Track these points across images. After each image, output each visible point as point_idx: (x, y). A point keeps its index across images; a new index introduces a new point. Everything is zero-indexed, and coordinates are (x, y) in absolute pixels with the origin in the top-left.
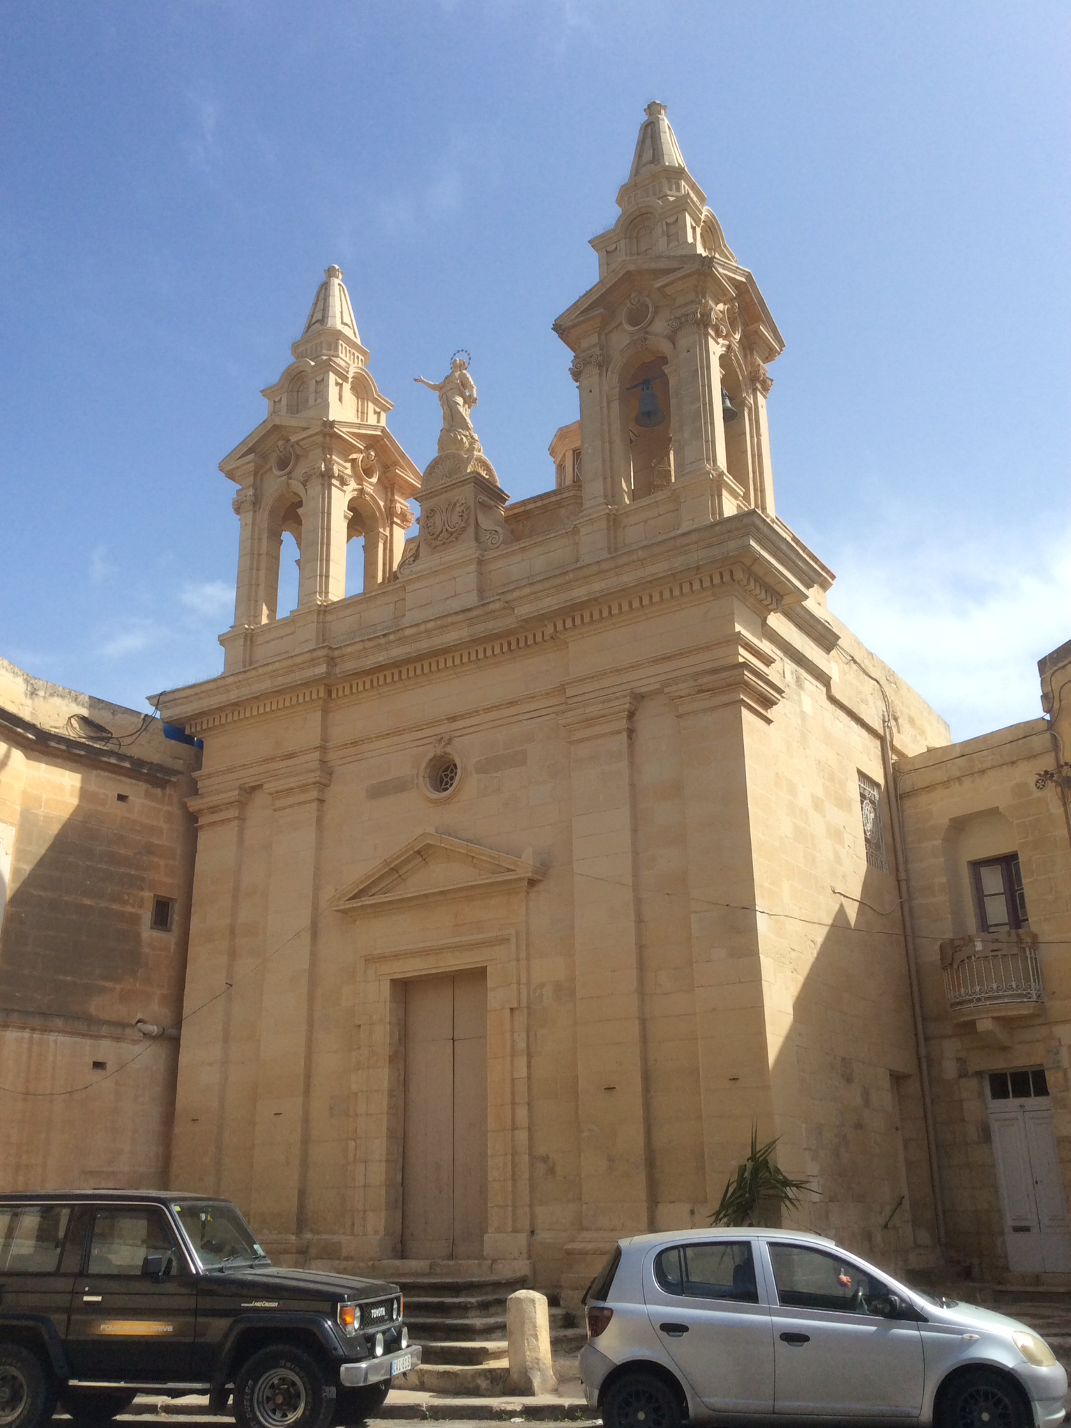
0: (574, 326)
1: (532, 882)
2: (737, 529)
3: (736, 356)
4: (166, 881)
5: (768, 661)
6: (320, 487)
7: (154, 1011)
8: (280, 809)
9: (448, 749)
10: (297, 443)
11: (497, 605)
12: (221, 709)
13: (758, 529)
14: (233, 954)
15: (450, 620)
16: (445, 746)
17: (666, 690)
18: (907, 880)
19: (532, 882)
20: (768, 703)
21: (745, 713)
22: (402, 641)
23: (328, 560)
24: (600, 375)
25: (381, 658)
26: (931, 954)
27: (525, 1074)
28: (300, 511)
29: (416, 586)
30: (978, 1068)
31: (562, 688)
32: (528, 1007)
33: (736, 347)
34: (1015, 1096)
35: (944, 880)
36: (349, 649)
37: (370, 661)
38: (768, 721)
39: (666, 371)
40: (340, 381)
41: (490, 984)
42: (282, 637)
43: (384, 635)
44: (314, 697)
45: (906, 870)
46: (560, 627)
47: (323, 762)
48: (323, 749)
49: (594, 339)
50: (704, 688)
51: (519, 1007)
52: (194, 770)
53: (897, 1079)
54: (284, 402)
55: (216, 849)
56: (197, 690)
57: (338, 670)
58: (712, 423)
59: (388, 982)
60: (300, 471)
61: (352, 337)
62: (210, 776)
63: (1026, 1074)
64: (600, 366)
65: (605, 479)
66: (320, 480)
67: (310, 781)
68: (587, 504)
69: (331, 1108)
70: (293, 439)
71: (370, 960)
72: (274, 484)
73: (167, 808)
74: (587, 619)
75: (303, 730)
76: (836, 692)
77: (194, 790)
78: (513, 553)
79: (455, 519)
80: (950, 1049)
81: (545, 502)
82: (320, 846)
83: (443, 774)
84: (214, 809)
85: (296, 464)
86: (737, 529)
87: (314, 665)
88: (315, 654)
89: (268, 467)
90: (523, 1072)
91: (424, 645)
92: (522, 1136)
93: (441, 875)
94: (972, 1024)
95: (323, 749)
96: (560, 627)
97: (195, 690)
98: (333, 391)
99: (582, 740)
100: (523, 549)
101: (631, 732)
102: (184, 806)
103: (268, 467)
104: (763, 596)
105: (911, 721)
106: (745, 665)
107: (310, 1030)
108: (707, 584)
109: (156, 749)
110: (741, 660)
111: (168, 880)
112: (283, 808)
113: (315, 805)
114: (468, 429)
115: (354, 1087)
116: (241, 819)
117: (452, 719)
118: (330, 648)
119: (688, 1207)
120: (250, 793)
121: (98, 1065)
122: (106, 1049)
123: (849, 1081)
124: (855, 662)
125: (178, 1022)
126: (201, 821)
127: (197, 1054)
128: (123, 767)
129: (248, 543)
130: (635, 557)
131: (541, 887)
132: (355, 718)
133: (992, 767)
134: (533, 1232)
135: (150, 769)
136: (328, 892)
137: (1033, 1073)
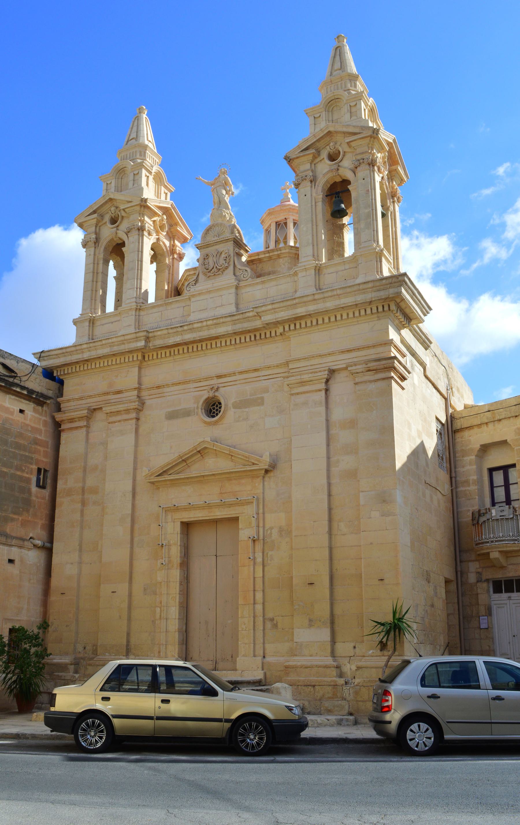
0: (297, 158)
1: (267, 471)
2: (395, 283)
3: (385, 183)
4: (46, 462)
5: (404, 356)
6: (137, 236)
7: (38, 533)
8: (112, 423)
9: (216, 394)
10: (124, 210)
11: (251, 314)
12: (77, 363)
13: (406, 283)
14: (84, 503)
15: (221, 320)
16: (214, 392)
17: (349, 369)
18: (455, 477)
19: (267, 471)
20: (403, 379)
21: (394, 384)
22: (192, 330)
23: (141, 279)
24: (311, 187)
25: (178, 339)
26: (467, 518)
27: (261, 575)
28: (124, 249)
29: (198, 298)
30: (487, 578)
31: (287, 363)
32: (263, 540)
33: (386, 177)
34: (506, 592)
35: (475, 477)
36: (159, 333)
37: (171, 341)
38: (403, 389)
39: (350, 189)
40: (148, 174)
41: (240, 526)
42: (112, 323)
43: (181, 326)
44: (135, 359)
45: (455, 472)
46: (287, 328)
47: (138, 397)
48: (139, 389)
49: (308, 166)
50: (371, 368)
51: (258, 539)
52: (58, 397)
53: (447, 582)
54: (113, 185)
55: (72, 444)
56: (64, 351)
57: (151, 345)
58: (377, 221)
59: (179, 523)
60: (124, 226)
61: (152, 148)
62: (68, 401)
63: (513, 580)
64: (311, 182)
65: (313, 246)
66: (137, 232)
67: (132, 407)
68: (301, 259)
69: (145, 590)
70: (122, 207)
71: (167, 510)
72: (108, 232)
73: (44, 418)
74: (303, 325)
75: (127, 378)
76: (428, 374)
77: (59, 409)
78: (257, 283)
79: (222, 261)
80: (473, 567)
81: (271, 254)
82: (136, 445)
83: (213, 408)
84: (72, 420)
85: (121, 222)
86: (395, 283)
87: (137, 341)
88: (138, 335)
89: (104, 221)
90: (259, 573)
91: (205, 334)
92: (259, 607)
93: (212, 464)
94: (488, 554)
95: (139, 389)
96: (287, 328)
97: (64, 351)
98: (144, 179)
99: (298, 394)
100: (263, 282)
101: (327, 390)
102: (53, 418)
103: (104, 221)
104: (403, 320)
105: (458, 390)
106: (395, 358)
107: (132, 547)
108: (374, 310)
109: (38, 384)
110: (393, 355)
111: (45, 460)
112: (115, 422)
113: (134, 421)
114: (228, 209)
115: (159, 579)
116: (88, 427)
117: (219, 377)
118: (147, 332)
119: (352, 645)
120: (93, 412)
121: (11, 561)
122: (15, 552)
123: (429, 582)
124: (436, 356)
125: (51, 539)
126: (63, 427)
127: (63, 557)
128: (23, 394)
129: (91, 266)
130: (335, 293)
131: (271, 474)
132: (161, 372)
133: (505, 418)
134: (264, 657)
135: (37, 395)
136: (143, 472)
137: (505, 581)
